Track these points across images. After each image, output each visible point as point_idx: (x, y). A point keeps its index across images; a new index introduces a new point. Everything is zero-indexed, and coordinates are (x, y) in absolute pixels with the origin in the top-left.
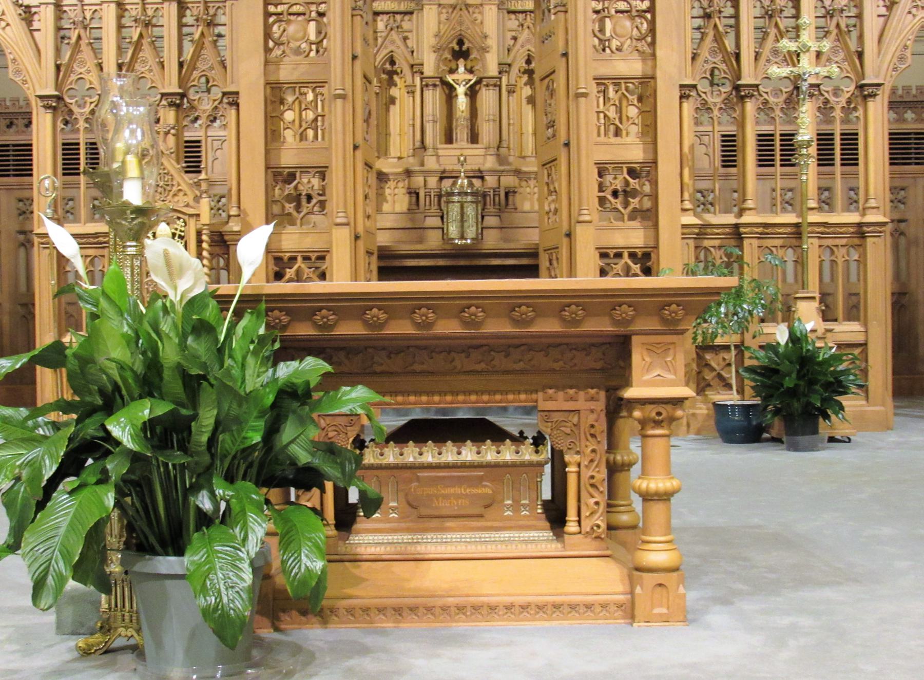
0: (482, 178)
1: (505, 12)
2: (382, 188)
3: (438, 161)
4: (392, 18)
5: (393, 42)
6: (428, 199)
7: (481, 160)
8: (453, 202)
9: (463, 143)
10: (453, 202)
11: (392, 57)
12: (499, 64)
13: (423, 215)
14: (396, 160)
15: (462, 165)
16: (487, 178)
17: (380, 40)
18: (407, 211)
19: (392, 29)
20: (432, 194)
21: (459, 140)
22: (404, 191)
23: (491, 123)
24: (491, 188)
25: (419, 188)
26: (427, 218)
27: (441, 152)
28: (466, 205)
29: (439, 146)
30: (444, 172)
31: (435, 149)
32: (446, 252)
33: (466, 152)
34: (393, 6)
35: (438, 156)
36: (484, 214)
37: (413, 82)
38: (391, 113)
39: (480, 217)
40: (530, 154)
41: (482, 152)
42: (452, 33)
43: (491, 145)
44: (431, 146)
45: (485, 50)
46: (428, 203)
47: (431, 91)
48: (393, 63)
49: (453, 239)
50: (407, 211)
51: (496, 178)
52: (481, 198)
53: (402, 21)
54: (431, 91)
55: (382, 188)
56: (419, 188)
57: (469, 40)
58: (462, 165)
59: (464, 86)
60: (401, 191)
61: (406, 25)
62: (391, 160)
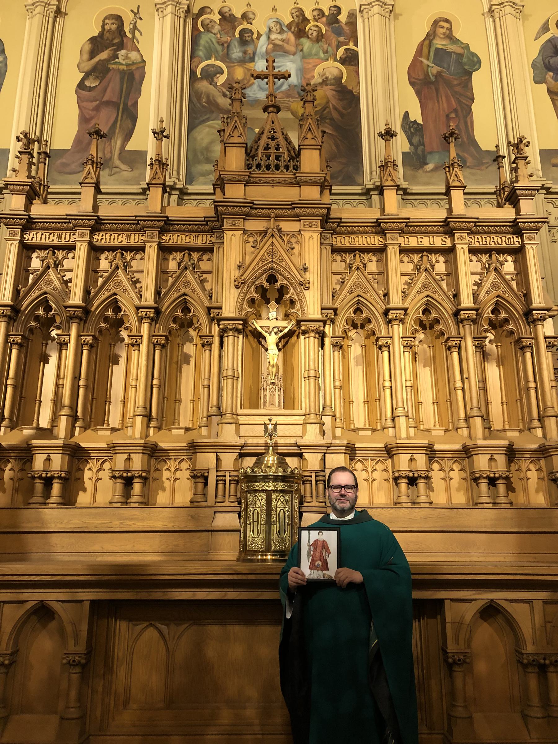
0: (300, 455)
1: (328, 247)
2: (158, 470)
3: (237, 431)
4: (187, 255)
5: (187, 284)
6: (221, 486)
7: (298, 430)
8: (256, 491)
9: (272, 407)
10: (256, 491)
11: (185, 302)
12: (322, 309)
13: (213, 510)
14: (182, 432)
15: (271, 435)
16: (306, 455)
17: (100, 280)
18: (189, 504)
19: (186, 268)
20: (227, 479)
21: (267, 404)
22: (187, 474)
23: (312, 381)
24: (311, 471)
25: (208, 471)
26: (217, 514)
27: (242, 420)
28: (274, 496)
29: (239, 411)
30: (243, 446)
31: (235, 414)
32: (240, 577)
33: (275, 419)
34: (188, 241)
35: (238, 425)
36: (303, 509)
37: (211, 332)
38: (184, 375)
39: (296, 514)
40: (361, 426)
41: (300, 419)
42: (261, 264)
43: (313, 411)
44: (229, 410)
45: (305, 285)
46: (220, 493)
47: (231, 338)
48: (186, 310)
49: (255, 553)
50: (189, 504)
51: (320, 456)
52: (492, 482)
53: (199, 260)
54: (231, 338)
55: (158, 470)
56: (208, 471)
57: (283, 276)
58: (271, 435)
59: (276, 333)
60: (184, 475)
61: (204, 265)
62: (174, 432)
